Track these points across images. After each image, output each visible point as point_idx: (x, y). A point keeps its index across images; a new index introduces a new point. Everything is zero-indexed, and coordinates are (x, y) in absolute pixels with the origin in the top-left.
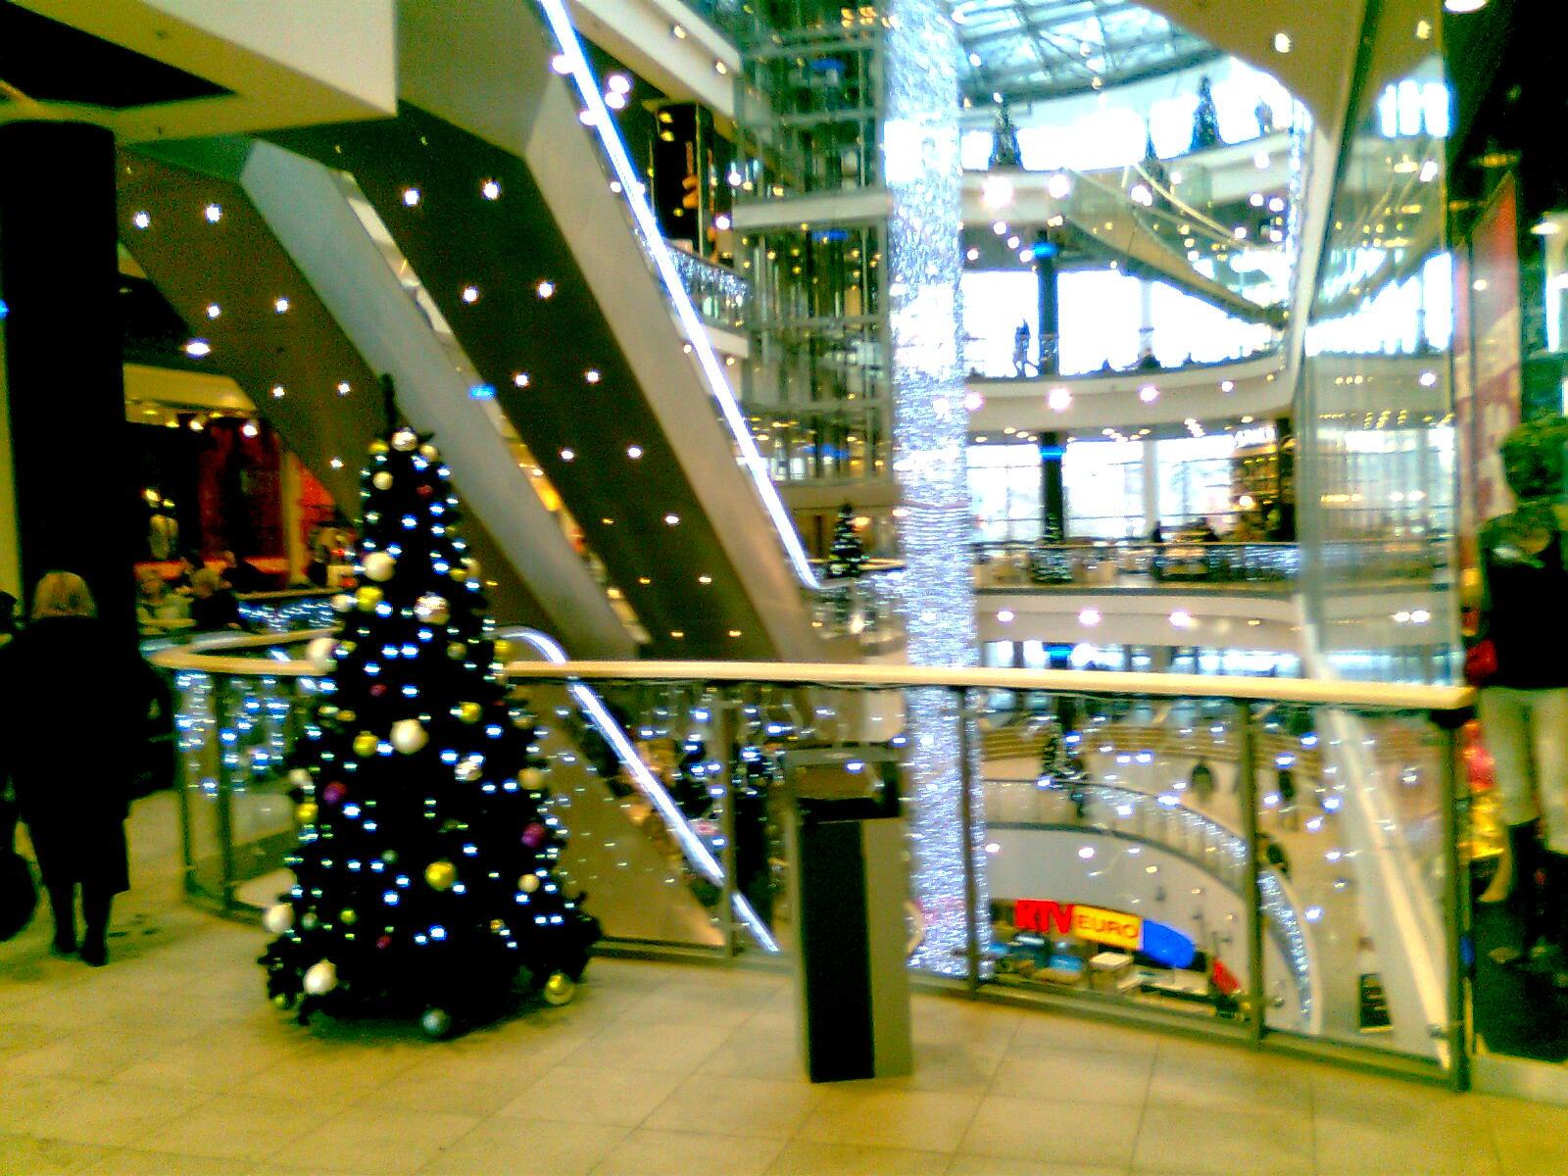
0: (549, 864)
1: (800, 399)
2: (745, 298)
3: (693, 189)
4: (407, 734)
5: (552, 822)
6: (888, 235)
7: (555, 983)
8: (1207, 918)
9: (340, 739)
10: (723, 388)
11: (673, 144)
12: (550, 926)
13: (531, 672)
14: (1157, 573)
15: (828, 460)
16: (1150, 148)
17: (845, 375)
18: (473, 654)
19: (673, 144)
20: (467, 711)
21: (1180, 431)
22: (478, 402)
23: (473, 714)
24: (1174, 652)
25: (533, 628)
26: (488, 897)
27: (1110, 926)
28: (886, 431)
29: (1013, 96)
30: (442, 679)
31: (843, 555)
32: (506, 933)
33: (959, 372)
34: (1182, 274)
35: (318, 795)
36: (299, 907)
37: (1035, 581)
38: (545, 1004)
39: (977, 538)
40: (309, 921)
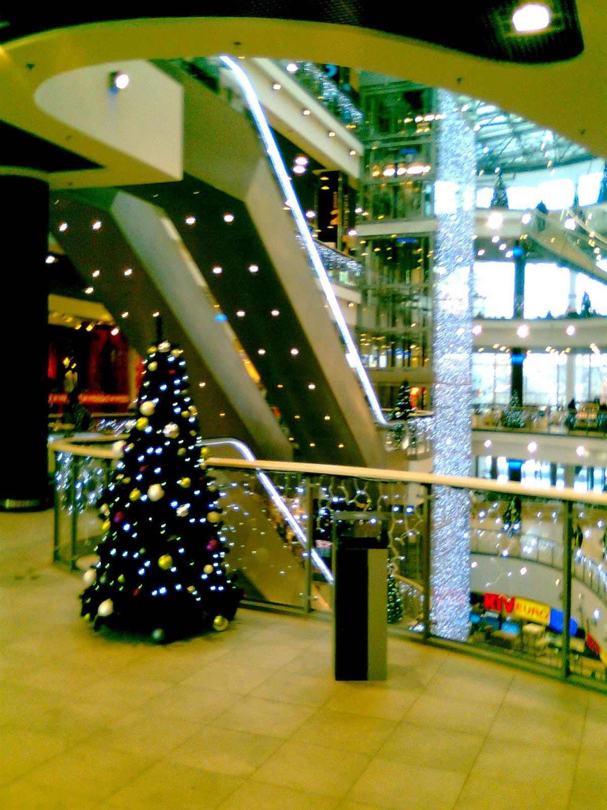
0: (220, 560)
1: (385, 326)
2: (361, 272)
3: (335, 216)
4: (155, 491)
5: (223, 539)
6: (435, 242)
7: (217, 620)
8: (584, 610)
9: (123, 491)
10: (342, 319)
11: (324, 193)
12: (217, 591)
13: (220, 464)
14: (570, 425)
15: (399, 357)
16: (576, 200)
17: (410, 314)
18: (188, 453)
19: (324, 193)
20: (184, 482)
21: (587, 350)
22: (219, 322)
23: (187, 483)
24: (578, 469)
25: (234, 438)
26: (189, 575)
27: (533, 611)
28: (429, 343)
29: (505, 169)
30: (175, 465)
31: (402, 408)
32: (195, 593)
33: (470, 314)
34: (589, 268)
35: (112, 517)
36: (99, 572)
37: (505, 425)
38: (213, 630)
39: (476, 401)
40: (103, 580)
